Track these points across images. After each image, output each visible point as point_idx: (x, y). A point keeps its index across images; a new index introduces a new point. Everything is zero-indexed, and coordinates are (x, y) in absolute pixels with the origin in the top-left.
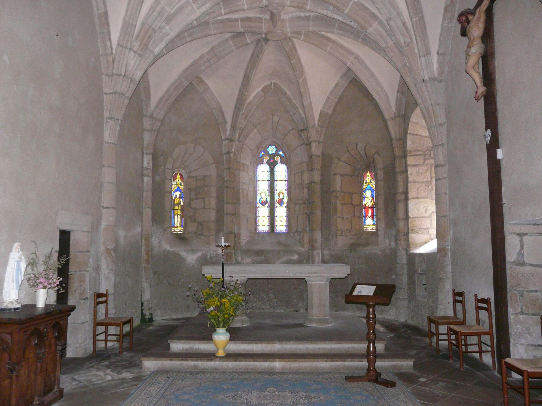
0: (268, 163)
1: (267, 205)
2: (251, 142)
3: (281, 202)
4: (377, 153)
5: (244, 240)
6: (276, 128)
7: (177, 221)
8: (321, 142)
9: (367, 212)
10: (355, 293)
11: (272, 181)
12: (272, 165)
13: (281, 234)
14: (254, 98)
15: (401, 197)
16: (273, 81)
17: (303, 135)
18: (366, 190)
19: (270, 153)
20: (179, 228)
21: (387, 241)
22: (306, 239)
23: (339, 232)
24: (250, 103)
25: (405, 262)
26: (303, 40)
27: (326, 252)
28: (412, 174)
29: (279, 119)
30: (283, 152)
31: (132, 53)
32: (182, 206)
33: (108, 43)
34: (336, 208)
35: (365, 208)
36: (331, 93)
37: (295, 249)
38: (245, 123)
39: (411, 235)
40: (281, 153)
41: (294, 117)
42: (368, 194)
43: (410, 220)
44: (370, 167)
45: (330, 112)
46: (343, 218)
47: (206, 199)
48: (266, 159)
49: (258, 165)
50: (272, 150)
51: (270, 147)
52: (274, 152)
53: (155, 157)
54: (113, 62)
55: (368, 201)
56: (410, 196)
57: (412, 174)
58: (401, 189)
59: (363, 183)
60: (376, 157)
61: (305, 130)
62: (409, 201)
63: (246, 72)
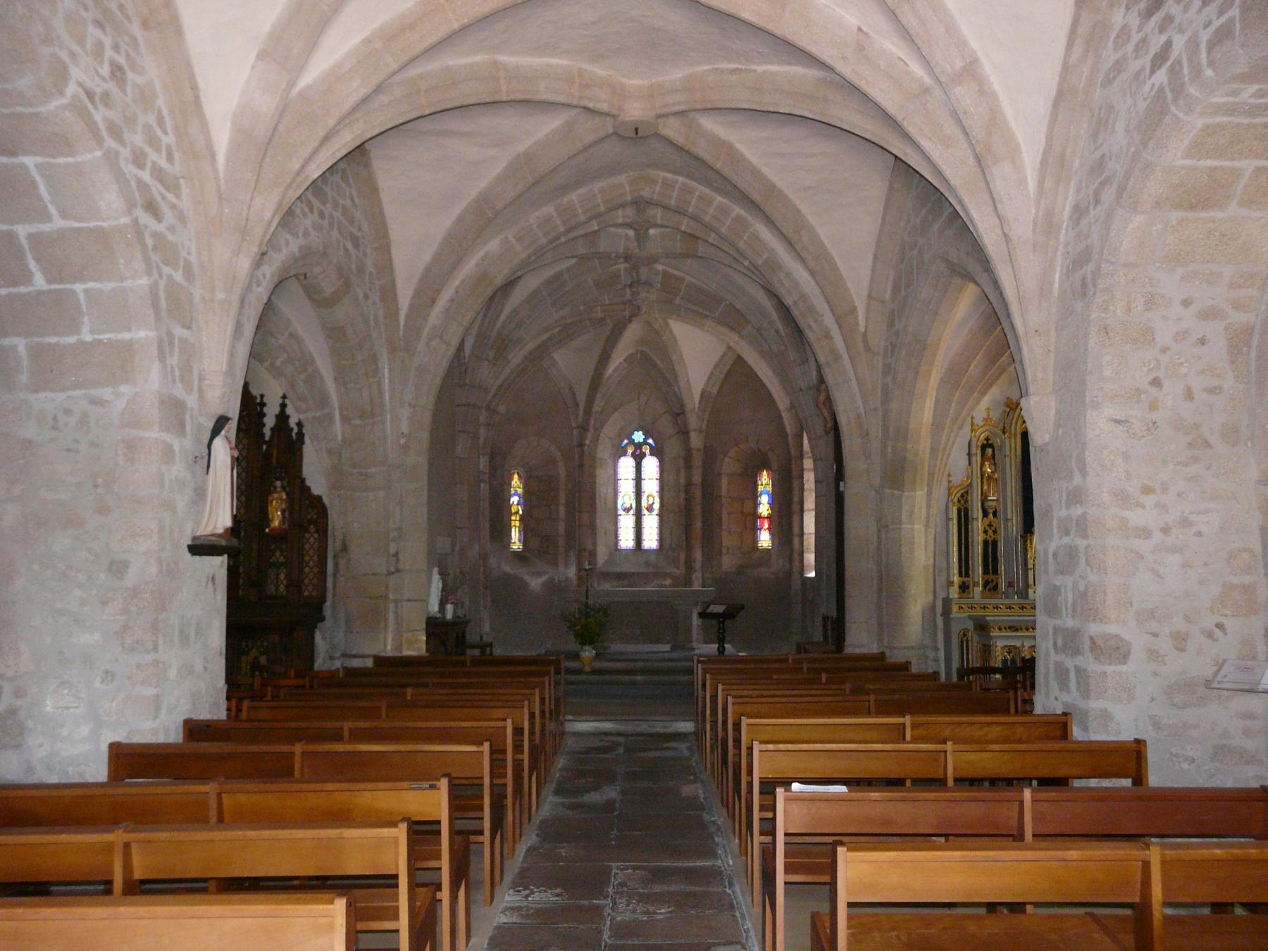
0: (633, 455)
1: (632, 512)
2: (609, 430)
3: (650, 509)
5: (601, 559)
7: (515, 534)
9: (762, 524)
10: (708, 611)
11: (638, 480)
12: (639, 458)
13: (649, 551)
15: (796, 507)
18: (761, 495)
19: (636, 441)
20: (518, 543)
21: (781, 562)
22: (682, 559)
23: (724, 550)
24: (610, 377)
25: (799, 587)
27: (708, 575)
28: (808, 481)
30: (654, 441)
31: (487, 363)
32: (521, 516)
34: (721, 519)
35: (760, 517)
36: (716, 366)
37: (668, 571)
39: (805, 554)
40: (650, 441)
42: (764, 499)
43: (805, 537)
44: (765, 465)
45: (715, 391)
46: (730, 532)
47: (553, 507)
49: (619, 458)
50: (638, 437)
51: (636, 432)
52: (642, 441)
53: (492, 457)
54: (466, 372)
55: (764, 509)
56: (805, 508)
57: (808, 481)
58: (796, 499)
59: (758, 485)
60: (770, 453)
61: (682, 413)
62: (805, 514)
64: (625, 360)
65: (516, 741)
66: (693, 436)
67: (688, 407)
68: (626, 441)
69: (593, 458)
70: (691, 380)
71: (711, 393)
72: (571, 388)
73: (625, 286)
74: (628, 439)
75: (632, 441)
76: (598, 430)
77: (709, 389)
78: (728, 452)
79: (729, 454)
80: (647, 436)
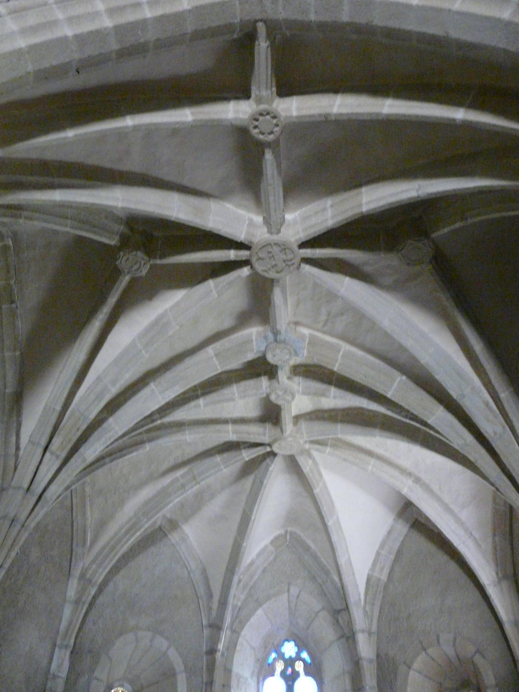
4: (478, 651)
6: (296, 608)
8: (374, 633)
14: (259, 555)
16: (289, 529)
17: (340, 619)
19: (287, 656)
24: (252, 563)
26: (329, 453)
29: (300, 591)
30: (309, 654)
33: (14, 438)
36: (382, 546)
38: (242, 597)
41: (324, 587)
45: (384, 577)
48: (280, 666)
49: (264, 679)
52: (294, 655)
60: (478, 659)
63: (244, 511)
64: (272, 542)
65: (443, 103)
66: (361, 639)
67: (352, 599)
68: (274, 655)
69: (228, 671)
70: (352, 558)
71: (379, 579)
72: (204, 572)
73: (295, 257)
74: (276, 652)
75: (281, 656)
76: (236, 632)
77: (376, 574)
78: (412, 662)
79: (415, 666)
80: (301, 645)
